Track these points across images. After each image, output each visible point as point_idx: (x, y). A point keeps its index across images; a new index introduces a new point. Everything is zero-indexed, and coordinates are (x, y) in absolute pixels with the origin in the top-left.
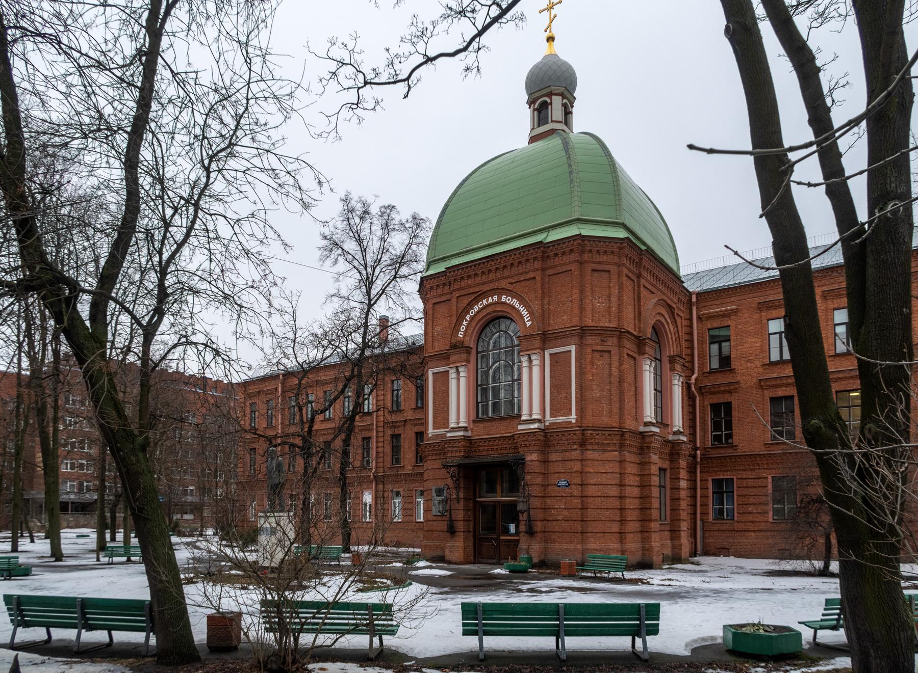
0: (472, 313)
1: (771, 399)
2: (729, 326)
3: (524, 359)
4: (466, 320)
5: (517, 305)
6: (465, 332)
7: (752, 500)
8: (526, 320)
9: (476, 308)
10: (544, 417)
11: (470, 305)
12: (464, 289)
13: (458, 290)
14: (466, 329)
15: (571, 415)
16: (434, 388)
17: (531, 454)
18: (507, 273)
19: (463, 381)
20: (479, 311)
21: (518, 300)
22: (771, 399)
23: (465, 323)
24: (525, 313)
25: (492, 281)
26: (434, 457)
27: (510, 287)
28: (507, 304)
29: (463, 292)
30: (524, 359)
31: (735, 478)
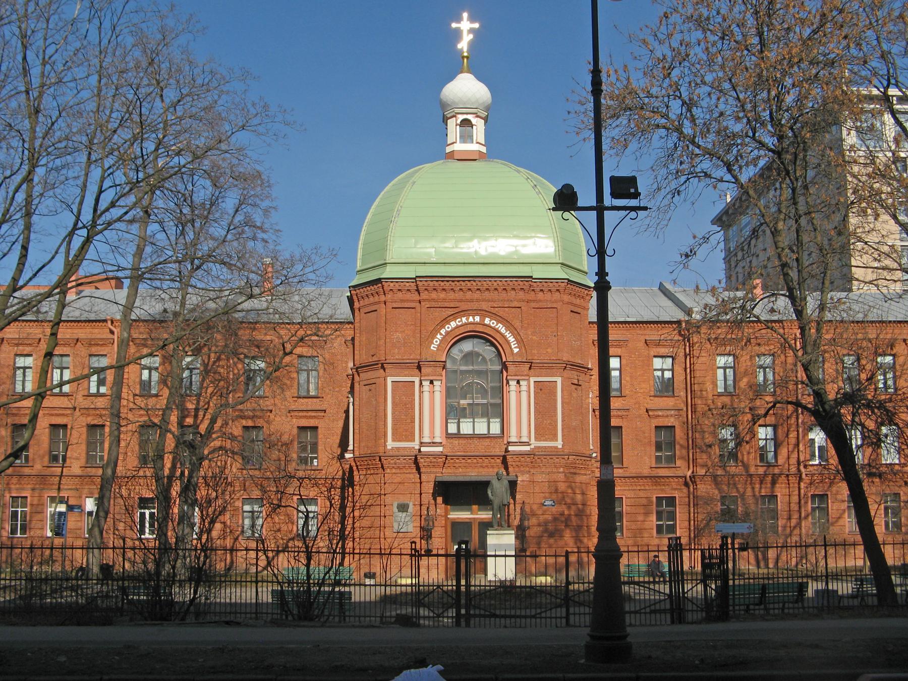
1: (656, 427)
3: (513, 383)
4: (441, 334)
5: (503, 330)
6: (439, 345)
8: (513, 347)
9: (453, 324)
10: (530, 440)
11: (446, 321)
12: (433, 300)
13: (428, 300)
15: (557, 440)
16: (393, 397)
17: (523, 474)
20: (457, 327)
21: (504, 326)
22: (656, 427)
23: (439, 336)
24: (511, 339)
25: (471, 301)
27: (492, 310)
28: (491, 327)
29: (434, 304)
30: (513, 383)
31: (624, 497)
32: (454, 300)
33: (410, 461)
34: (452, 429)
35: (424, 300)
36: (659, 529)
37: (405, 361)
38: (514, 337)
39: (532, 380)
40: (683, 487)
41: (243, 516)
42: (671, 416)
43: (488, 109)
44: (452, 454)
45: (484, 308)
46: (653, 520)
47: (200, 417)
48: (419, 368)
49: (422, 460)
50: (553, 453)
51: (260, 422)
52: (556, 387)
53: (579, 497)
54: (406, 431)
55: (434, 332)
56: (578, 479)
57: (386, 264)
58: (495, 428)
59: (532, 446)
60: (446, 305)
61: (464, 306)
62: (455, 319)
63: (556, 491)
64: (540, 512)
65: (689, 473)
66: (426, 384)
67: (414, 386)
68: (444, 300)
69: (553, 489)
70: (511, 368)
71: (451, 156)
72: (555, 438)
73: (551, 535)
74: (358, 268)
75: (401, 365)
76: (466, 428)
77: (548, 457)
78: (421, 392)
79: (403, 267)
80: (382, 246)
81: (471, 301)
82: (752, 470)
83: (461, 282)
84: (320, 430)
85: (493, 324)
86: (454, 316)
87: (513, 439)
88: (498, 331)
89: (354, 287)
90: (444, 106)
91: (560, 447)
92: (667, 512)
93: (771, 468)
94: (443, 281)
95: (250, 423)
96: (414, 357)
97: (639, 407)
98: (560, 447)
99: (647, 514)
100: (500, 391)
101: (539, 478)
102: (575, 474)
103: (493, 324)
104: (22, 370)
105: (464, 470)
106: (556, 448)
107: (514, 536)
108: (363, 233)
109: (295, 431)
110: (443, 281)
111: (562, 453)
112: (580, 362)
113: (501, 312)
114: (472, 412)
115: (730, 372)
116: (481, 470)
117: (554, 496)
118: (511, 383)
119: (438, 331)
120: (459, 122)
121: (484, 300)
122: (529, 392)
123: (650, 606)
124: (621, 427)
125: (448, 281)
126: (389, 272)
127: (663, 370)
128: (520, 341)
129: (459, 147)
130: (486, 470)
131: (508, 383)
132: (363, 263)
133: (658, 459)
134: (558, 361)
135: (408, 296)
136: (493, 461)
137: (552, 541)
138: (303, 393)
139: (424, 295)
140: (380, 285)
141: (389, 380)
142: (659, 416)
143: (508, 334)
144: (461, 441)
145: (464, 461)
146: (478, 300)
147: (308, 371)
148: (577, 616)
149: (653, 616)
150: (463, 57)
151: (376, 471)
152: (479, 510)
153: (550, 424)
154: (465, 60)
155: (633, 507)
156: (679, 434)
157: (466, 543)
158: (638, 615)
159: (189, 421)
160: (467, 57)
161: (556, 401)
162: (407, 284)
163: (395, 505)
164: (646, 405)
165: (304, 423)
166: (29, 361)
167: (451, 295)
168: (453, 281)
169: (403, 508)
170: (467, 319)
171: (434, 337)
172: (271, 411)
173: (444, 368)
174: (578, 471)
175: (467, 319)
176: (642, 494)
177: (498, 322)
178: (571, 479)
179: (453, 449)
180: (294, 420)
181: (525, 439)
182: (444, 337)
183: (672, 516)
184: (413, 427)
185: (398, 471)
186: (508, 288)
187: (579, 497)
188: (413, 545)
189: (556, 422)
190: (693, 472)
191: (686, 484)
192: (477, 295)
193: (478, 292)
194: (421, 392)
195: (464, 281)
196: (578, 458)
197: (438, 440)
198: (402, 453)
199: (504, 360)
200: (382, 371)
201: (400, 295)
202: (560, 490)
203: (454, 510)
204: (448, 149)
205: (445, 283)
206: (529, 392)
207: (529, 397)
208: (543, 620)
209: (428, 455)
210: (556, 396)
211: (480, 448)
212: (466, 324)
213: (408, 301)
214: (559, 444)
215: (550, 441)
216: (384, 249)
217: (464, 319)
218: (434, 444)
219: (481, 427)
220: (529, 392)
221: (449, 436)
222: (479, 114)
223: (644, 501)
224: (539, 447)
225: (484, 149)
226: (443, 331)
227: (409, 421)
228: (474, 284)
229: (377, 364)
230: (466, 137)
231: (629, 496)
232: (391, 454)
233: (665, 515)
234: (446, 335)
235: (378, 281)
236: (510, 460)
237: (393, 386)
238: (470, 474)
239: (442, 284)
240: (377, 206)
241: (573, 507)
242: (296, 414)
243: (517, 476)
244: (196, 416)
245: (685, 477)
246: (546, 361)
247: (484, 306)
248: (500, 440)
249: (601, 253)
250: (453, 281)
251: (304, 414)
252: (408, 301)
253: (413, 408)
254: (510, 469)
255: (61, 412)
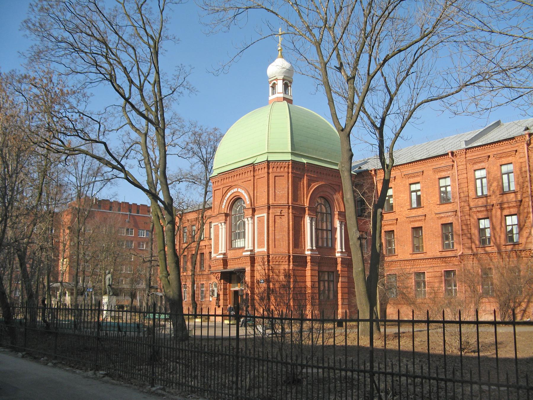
31: (426, 272)
42: (450, 216)
72: (258, 247)
82: (503, 248)
93: (517, 246)
97: (432, 212)
104: (506, 175)
115: (484, 181)
124: (393, 231)
127: (446, 187)
142: (442, 217)
164: (435, 211)
166: (510, 167)
249: (402, 128)
255: (414, 219)
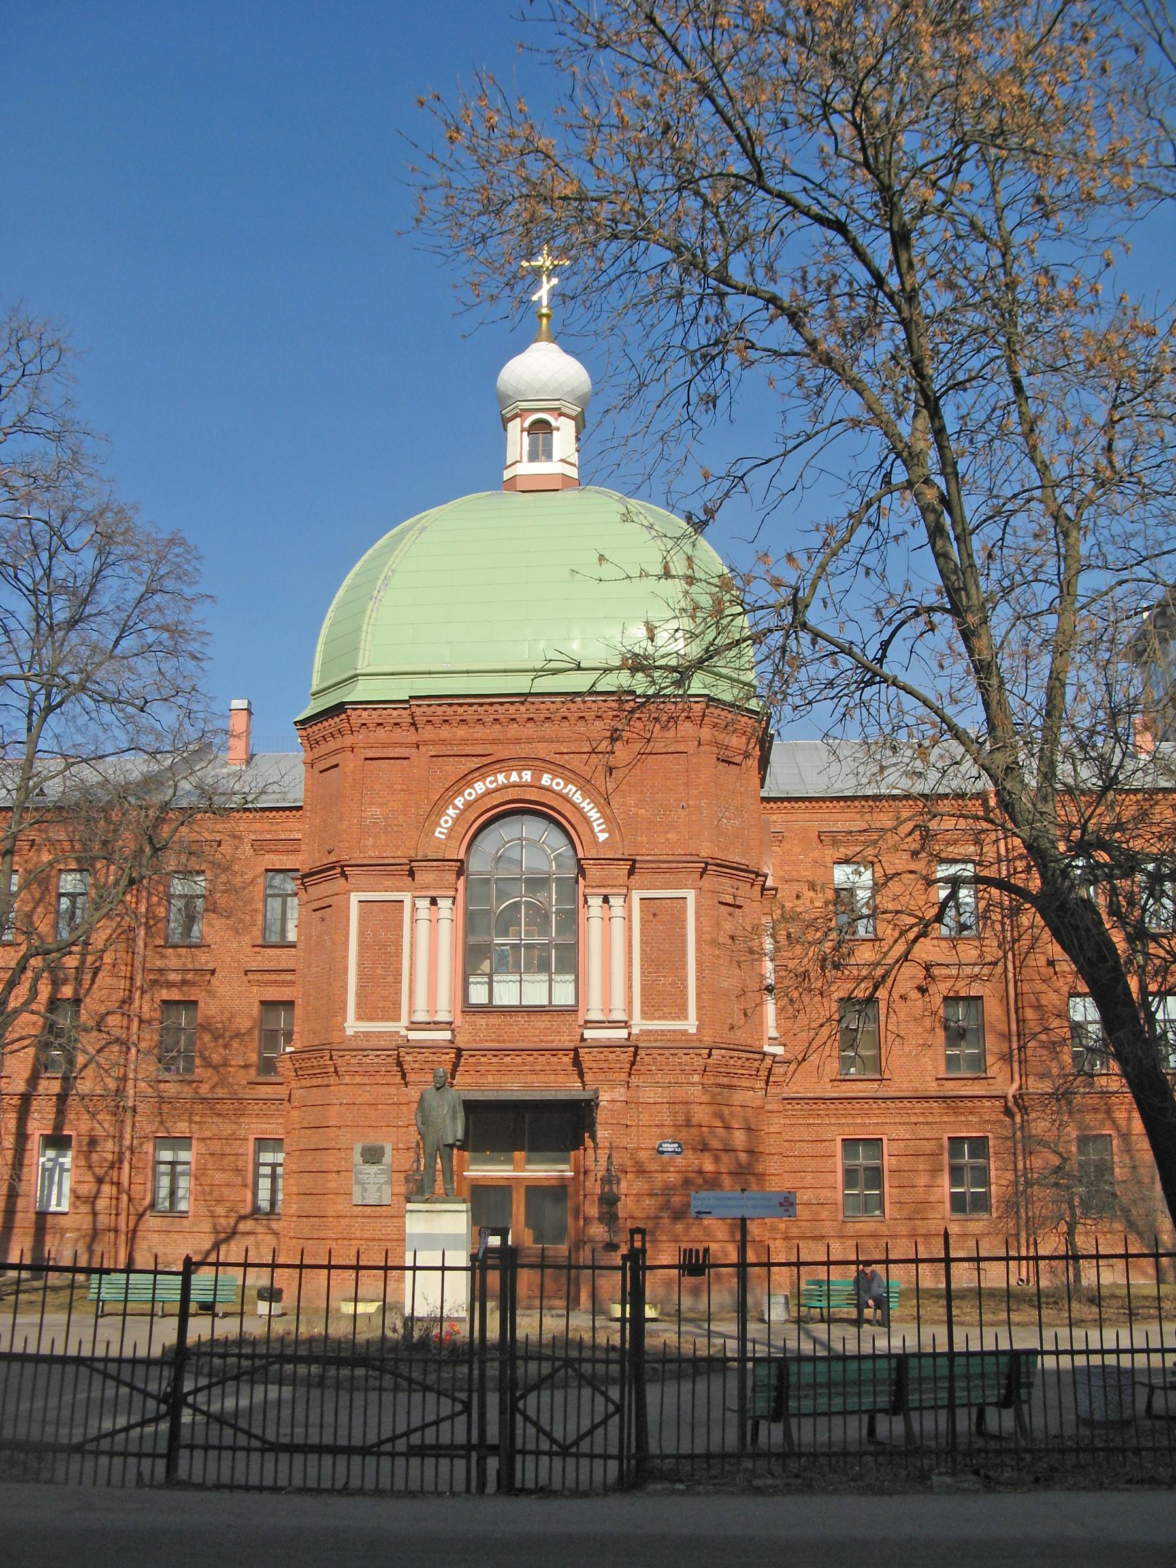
0: (470, 794)
2: (195, 1003)
3: (595, 902)
4: (455, 807)
5: (577, 798)
6: (451, 829)
7: (701, 1414)
8: (597, 829)
9: (480, 787)
10: (630, 1016)
11: (465, 780)
12: (443, 742)
13: (434, 743)
14: (454, 825)
15: (686, 1018)
17: (613, 1087)
18: (548, 729)
19: (445, 928)
20: (489, 793)
21: (580, 788)
22: (946, 998)
23: (451, 812)
24: (594, 814)
25: (518, 741)
26: (358, 1079)
27: (558, 759)
28: (553, 792)
29: (445, 750)
30: (595, 902)
32: (484, 742)
33: (390, 1060)
34: (478, 995)
35: (426, 743)
36: (958, 1203)
37: (387, 861)
38: (599, 811)
39: (636, 896)
40: (1002, 1117)
41: (154, 1170)
43: (584, 401)
44: (474, 1046)
45: (542, 755)
46: (945, 1187)
47: (86, 983)
48: (412, 874)
49: (409, 1058)
50: (677, 1044)
51: (194, 994)
52: (684, 909)
53: (739, 1138)
54: (384, 998)
55: (441, 803)
56: (739, 1097)
57: (356, 676)
58: (564, 994)
59: (635, 1030)
60: (468, 750)
61: (501, 752)
62: (483, 777)
63: (688, 1124)
64: (654, 1167)
65: (1012, 1090)
66: (424, 904)
67: (402, 910)
68: (464, 741)
69: (681, 1119)
70: (593, 872)
71: (511, 484)
72: (682, 1014)
73: (679, 1215)
74: (314, 688)
75: (381, 869)
76: (507, 993)
77: (666, 1052)
78: (414, 921)
79: (388, 682)
80: (349, 644)
81: (518, 741)
83: (497, 707)
84: (298, 1011)
85: (558, 784)
86: (481, 772)
87: (595, 1015)
88: (566, 799)
89: (302, 722)
90: (502, 399)
91: (693, 1030)
92: (973, 1168)
94: (460, 705)
95: (175, 995)
96: (400, 853)
98: (693, 1030)
99: (935, 1171)
100: (571, 920)
101: (650, 1095)
102: (730, 1087)
103: (558, 784)
105: (498, 1079)
106: (685, 1033)
107: (464, 1216)
108: (327, 623)
109: (256, 1009)
110: (460, 705)
111: (697, 1044)
112: (737, 859)
113: (575, 762)
114: (509, 963)
116: (531, 1078)
117: (684, 1134)
118: (591, 901)
119: (450, 802)
120: (527, 424)
121: (542, 740)
122: (630, 920)
123: (407, 1434)
125: (471, 705)
126: (360, 692)
128: (608, 819)
129: (526, 468)
130: (541, 1078)
131: (586, 902)
132: (322, 679)
133: (951, 1061)
134: (689, 858)
135: (399, 735)
136: (554, 1059)
137: (679, 1227)
138: (274, 938)
139: (427, 733)
140: (343, 716)
141: (355, 898)
143: (586, 805)
144: (494, 1020)
145: (495, 1060)
146: (529, 741)
147: (284, 897)
148: (199, 1454)
149: (415, 1462)
150: (541, 316)
151: (326, 1081)
152: (529, 1161)
153: (673, 984)
154: (545, 321)
155: (903, 1159)
156: (993, 1010)
157: (503, 1233)
158: (371, 1461)
159: (67, 991)
160: (548, 316)
161: (684, 936)
162: (395, 713)
163: (358, 1148)
165: (273, 994)
167: (480, 732)
168: (481, 705)
169: (373, 1155)
170: (507, 777)
171: (441, 813)
172: (213, 972)
173: (460, 872)
174: (735, 1082)
175: (507, 777)
176: (926, 1132)
177: (568, 781)
178: (720, 1099)
179: (476, 1035)
180: (255, 989)
181: (618, 1015)
182: (463, 812)
183: (982, 1178)
184: (398, 992)
185: (366, 1080)
186: (590, 715)
187: (739, 1138)
188: (638, 1237)
189: (684, 980)
190: (1020, 1088)
191: (1008, 1112)
192: (529, 730)
193: (529, 725)
194: (414, 921)
195: (502, 704)
196: (736, 1054)
197: (443, 1017)
198: (374, 1043)
199: (581, 855)
200: (342, 880)
201: (381, 734)
202: (695, 1121)
203: (475, 1161)
204: (507, 474)
205: (466, 708)
206: (628, 919)
207: (630, 929)
208: (104, 1460)
209: (421, 1047)
210: (684, 927)
211: (533, 1032)
212: (505, 787)
213: (396, 744)
214: (690, 1024)
215: (673, 1019)
216: (353, 650)
217: (501, 778)
218: (435, 1025)
219: (535, 992)
220: (628, 919)
221: (469, 1009)
222: (564, 410)
223: (928, 1147)
224: (650, 1032)
225: (573, 473)
226: (459, 802)
227: (390, 979)
228: (523, 709)
229: (333, 868)
230: (541, 450)
231: (894, 1136)
232: (353, 1045)
233: (968, 1175)
234: (465, 810)
235: (339, 708)
236: (586, 1057)
237: (361, 910)
238: (509, 1086)
239: (460, 710)
240: (357, 575)
241: (725, 1158)
242: (258, 976)
243: (596, 1091)
244: (79, 981)
245: (1005, 1097)
246: (665, 858)
247: (542, 750)
248: (570, 1018)
250: (481, 705)
251: (274, 977)
252: (396, 744)
253: (399, 954)
254: (587, 1077)
